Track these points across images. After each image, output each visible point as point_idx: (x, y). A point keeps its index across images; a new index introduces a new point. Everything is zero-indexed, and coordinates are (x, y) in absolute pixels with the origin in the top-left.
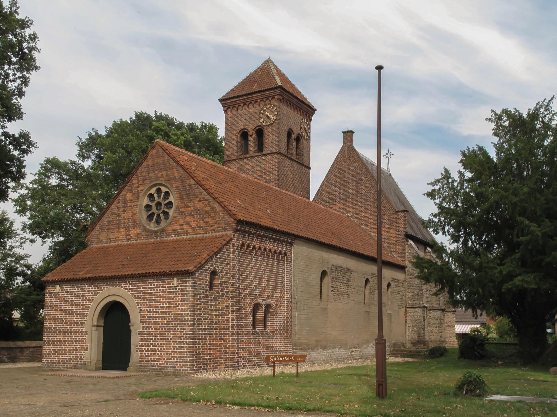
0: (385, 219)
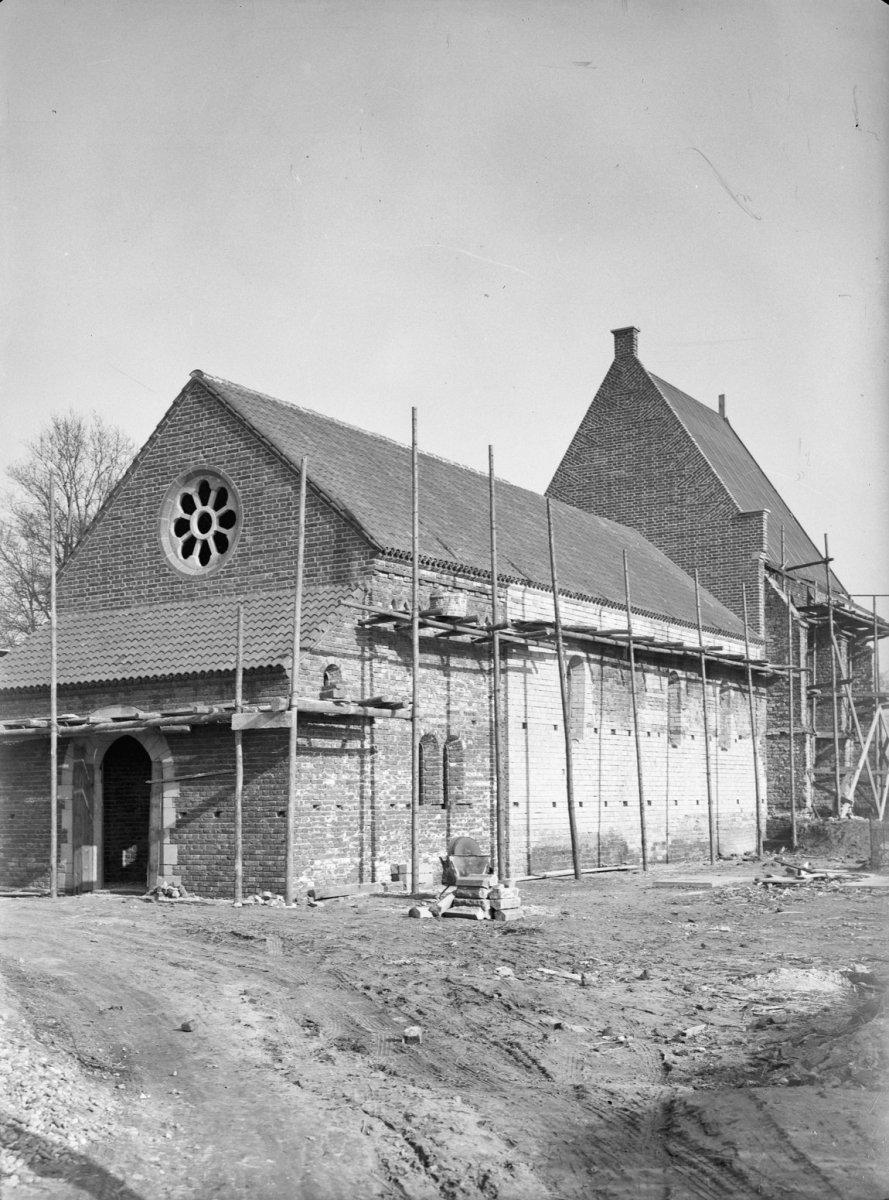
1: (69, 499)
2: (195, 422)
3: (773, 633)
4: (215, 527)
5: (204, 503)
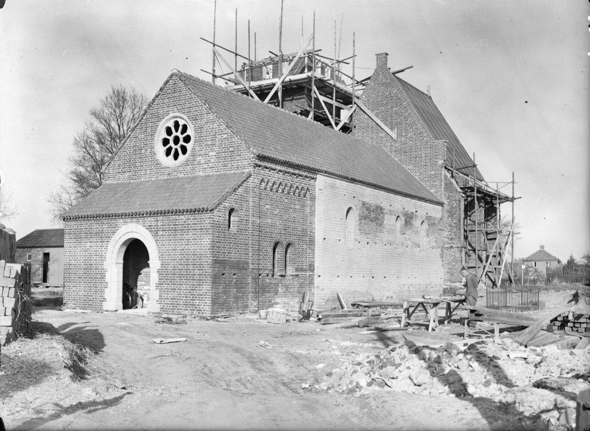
0: (288, 263)
1: (119, 127)
2: (173, 93)
4: (181, 142)
5: (177, 131)
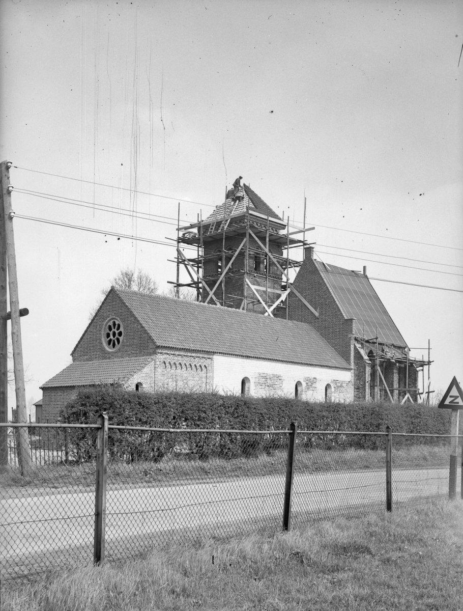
3: (356, 365)
